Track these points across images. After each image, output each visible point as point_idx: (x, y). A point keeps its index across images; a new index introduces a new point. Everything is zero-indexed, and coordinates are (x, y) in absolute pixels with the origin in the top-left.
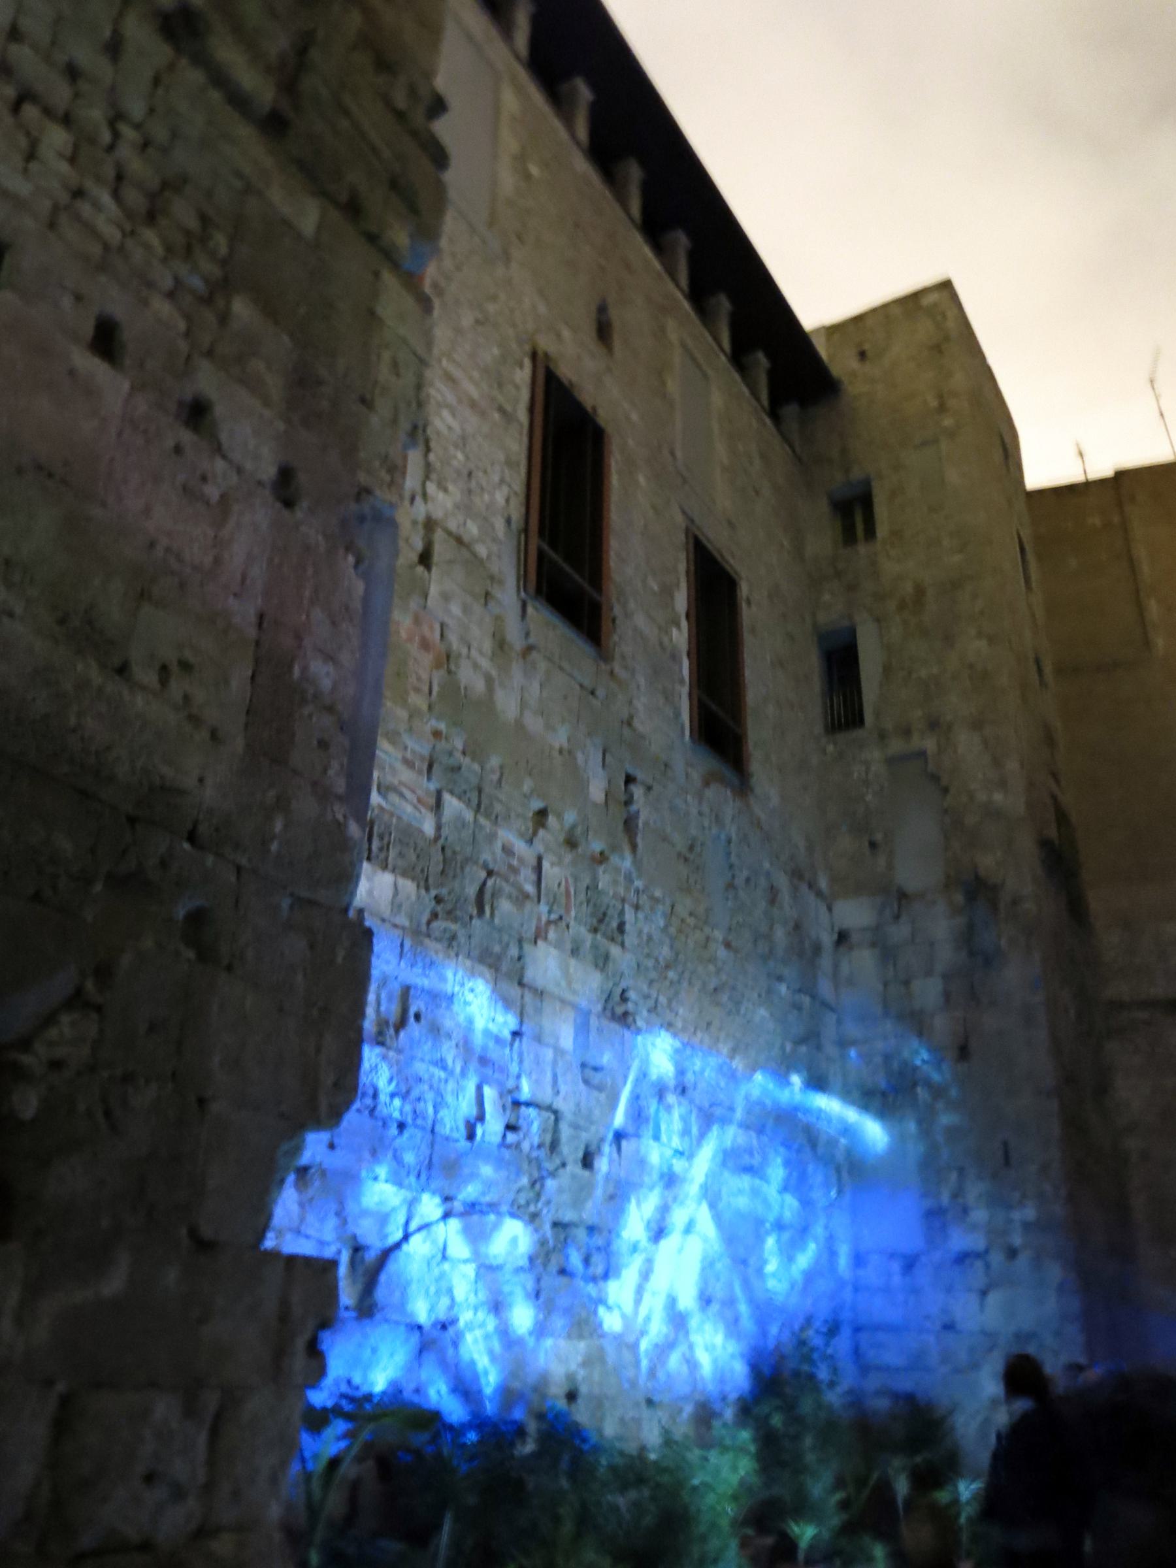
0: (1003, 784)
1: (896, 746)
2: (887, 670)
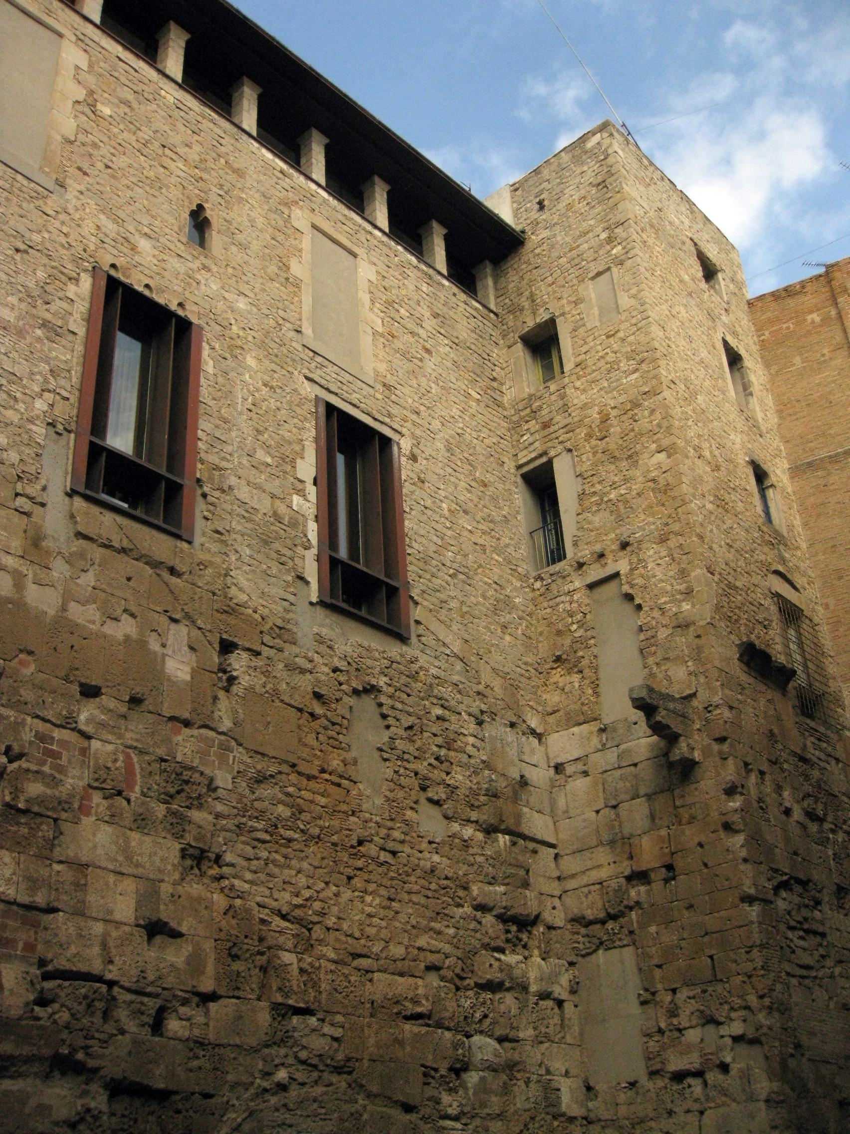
0: (688, 593)
1: (595, 573)
2: (582, 496)
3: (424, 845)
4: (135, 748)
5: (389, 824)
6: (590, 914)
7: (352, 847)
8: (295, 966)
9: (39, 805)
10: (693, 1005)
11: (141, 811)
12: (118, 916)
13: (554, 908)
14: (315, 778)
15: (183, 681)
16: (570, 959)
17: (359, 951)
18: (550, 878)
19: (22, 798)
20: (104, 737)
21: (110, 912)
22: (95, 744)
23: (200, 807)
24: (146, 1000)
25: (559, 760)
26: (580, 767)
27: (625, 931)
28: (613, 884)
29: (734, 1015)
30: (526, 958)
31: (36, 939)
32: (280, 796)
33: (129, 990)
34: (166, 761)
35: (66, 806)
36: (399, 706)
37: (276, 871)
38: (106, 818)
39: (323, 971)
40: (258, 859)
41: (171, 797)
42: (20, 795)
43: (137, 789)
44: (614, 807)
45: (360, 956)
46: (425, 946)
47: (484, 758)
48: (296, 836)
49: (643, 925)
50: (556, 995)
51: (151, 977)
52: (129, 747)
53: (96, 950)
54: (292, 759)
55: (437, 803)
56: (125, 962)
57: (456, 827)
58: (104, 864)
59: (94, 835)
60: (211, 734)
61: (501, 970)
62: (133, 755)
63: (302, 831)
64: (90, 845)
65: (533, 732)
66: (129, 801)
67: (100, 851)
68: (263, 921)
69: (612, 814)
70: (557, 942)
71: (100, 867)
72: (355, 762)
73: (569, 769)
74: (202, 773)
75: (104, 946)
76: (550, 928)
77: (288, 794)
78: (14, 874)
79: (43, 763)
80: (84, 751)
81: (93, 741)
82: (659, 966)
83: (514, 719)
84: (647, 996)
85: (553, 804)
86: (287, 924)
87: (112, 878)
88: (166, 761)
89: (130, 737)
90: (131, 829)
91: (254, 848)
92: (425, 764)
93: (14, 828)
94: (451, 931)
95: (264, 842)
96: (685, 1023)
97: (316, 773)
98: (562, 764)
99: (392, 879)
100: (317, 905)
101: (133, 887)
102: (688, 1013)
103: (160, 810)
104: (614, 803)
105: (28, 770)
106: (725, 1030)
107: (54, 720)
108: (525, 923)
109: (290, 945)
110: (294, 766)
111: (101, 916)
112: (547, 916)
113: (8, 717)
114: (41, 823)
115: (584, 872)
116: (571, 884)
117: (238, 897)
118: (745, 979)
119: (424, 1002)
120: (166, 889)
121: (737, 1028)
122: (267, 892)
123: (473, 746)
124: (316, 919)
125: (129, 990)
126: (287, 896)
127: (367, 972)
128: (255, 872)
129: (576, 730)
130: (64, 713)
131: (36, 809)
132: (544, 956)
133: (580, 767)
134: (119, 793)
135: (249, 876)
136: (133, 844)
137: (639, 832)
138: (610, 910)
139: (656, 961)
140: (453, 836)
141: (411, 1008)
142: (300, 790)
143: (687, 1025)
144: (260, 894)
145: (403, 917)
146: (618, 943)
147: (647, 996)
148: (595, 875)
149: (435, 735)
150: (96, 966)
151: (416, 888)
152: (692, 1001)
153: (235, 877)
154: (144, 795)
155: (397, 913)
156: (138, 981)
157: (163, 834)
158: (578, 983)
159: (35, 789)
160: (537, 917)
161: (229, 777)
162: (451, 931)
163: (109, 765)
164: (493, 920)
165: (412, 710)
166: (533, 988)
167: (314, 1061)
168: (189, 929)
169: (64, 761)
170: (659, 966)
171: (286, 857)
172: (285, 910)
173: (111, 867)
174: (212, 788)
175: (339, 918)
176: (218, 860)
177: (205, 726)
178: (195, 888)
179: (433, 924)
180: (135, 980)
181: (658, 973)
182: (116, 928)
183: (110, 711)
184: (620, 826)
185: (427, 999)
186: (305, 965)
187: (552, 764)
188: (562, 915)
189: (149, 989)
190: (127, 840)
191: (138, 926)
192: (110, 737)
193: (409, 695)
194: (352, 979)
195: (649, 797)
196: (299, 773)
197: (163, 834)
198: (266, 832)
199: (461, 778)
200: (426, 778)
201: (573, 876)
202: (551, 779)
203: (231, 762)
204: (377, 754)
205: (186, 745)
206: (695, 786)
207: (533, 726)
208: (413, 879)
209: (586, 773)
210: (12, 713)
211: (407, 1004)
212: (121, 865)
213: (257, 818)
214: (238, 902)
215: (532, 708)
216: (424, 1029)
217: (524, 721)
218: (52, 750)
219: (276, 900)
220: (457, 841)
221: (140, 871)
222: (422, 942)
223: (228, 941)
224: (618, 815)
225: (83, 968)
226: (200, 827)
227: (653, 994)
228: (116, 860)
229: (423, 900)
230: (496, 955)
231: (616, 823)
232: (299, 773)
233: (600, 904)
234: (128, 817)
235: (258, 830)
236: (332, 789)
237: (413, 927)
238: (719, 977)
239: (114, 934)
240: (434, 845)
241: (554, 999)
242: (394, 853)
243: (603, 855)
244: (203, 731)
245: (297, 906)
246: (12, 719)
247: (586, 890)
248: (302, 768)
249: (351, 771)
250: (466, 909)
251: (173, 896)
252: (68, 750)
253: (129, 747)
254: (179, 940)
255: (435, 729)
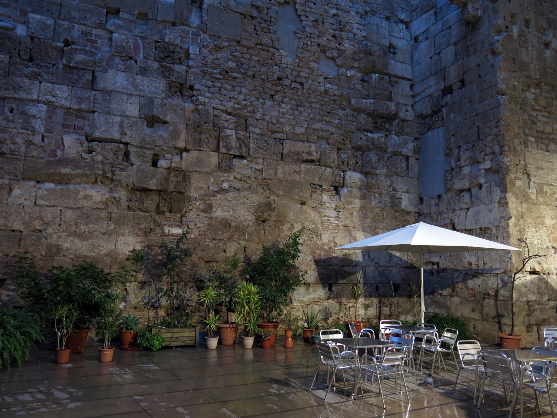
3: (321, 79)
4: (140, 36)
5: (298, 69)
6: (425, 112)
7: (274, 80)
8: (234, 136)
9: (83, 64)
10: (467, 154)
11: (143, 65)
12: (128, 114)
13: (407, 111)
14: (252, 48)
15: (170, 3)
16: (415, 136)
17: (275, 129)
18: (405, 96)
19: (72, 62)
20: (121, 32)
21: (124, 112)
22: (115, 35)
23: (181, 63)
24: (145, 151)
25: (416, 34)
26: (425, 35)
27: (440, 119)
28: (436, 95)
29: (486, 158)
30: (387, 136)
31: (84, 125)
32: (230, 57)
33: (136, 147)
34: (159, 42)
35: (99, 65)
36: (308, 10)
37: (225, 92)
38: (122, 70)
39: (251, 138)
40: (215, 87)
41: (163, 59)
42: (71, 60)
43: (141, 56)
44: (439, 53)
45: (275, 132)
46: (318, 128)
47: (364, 35)
48: (239, 76)
49: (448, 115)
50: (404, 153)
51: (147, 140)
52: (135, 36)
53: (117, 128)
54: (238, 38)
55: (333, 59)
56: (133, 134)
57: (343, 70)
58: (120, 90)
59: (115, 77)
60: (189, 28)
61: (367, 141)
62: (139, 40)
63: (243, 73)
64: (113, 82)
65: (402, 22)
66: (136, 62)
67: (118, 84)
68: (214, 116)
69: (436, 57)
70: (407, 128)
71: (119, 92)
72: (278, 40)
73: (420, 38)
74: (181, 48)
75: (121, 126)
76: (403, 121)
77: (234, 56)
78: (69, 96)
79: (86, 46)
80: (111, 39)
81: (114, 34)
82: (454, 135)
83: (389, 14)
84: (448, 151)
85: (412, 57)
86: (231, 117)
87: (125, 97)
88: (159, 42)
89: (136, 32)
90: (137, 74)
91: (212, 82)
92: (325, 39)
93: (71, 76)
94: (337, 121)
95: (218, 79)
96: (463, 164)
97: (253, 46)
98: (417, 36)
99: (299, 96)
100: (250, 109)
101: (137, 100)
102: (465, 158)
103: (156, 65)
104: (438, 51)
105: (76, 49)
106: (482, 166)
107: (91, 25)
108: (390, 118)
109: (231, 126)
110: (238, 42)
111: (119, 113)
112: (402, 115)
113: (64, 25)
114: (85, 73)
115: (423, 91)
116: (418, 98)
117: (201, 104)
118: (495, 138)
119: (314, 154)
120: (157, 102)
121: (488, 165)
122: (220, 102)
123: (357, 28)
124: (249, 114)
125: (136, 147)
126: (231, 104)
127: (280, 139)
128: (213, 93)
129: (424, 16)
130: (97, 21)
131: (81, 66)
132: (398, 134)
133: (425, 35)
134: (131, 58)
135: (208, 95)
136: (138, 81)
137: (449, 65)
138: (434, 109)
139: (452, 133)
140: (342, 75)
141: (305, 157)
142: (242, 54)
143: (464, 165)
144: (216, 103)
145: (305, 114)
146: (437, 126)
147: (448, 151)
148: (428, 92)
149: (332, 24)
150: (116, 135)
151: (314, 100)
152: (467, 152)
153: (200, 95)
154: (144, 58)
155: (301, 112)
156: (141, 142)
157: (156, 76)
158: (419, 148)
159: (80, 57)
160: (396, 114)
161: (198, 49)
162: (337, 121)
163: (124, 44)
164: (365, 116)
165: (316, 11)
166: (390, 149)
167: (244, 179)
168: (171, 119)
169: (99, 44)
170: (454, 135)
171: (232, 86)
172: (230, 110)
173: (124, 91)
174: (188, 54)
175: (264, 114)
176: (191, 88)
177: (184, 25)
178: (176, 101)
179: (324, 118)
180: (138, 142)
181: (453, 139)
182: (128, 119)
183: (125, 19)
184: (441, 63)
185: (317, 153)
186: (240, 136)
187: (413, 38)
188: (413, 114)
189: (147, 146)
190: (134, 80)
191: (140, 118)
192: (124, 32)
193: (315, 4)
194: (270, 143)
195: (455, 44)
196: (242, 46)
197: (156, 76)
198: (221, 74)
199: (348, 45)
200: (324, 46)
201: (419, 94)
202: (412, 46)
203: (199, 41)
204: (293, 35)
205: (171, 36)
206: (477, 32)
207: (402, 18)
208: (313, 96)
209: (427, 38)
210: (66, 23)
211: (304, 155)
212: (131, 91)
213: (216, 68)
214: (201, 107)
215: (403, 8)
216: (313, 167)
217: (396, 16)
218: (92, 39)
219: (225, 106)
220: (343, 77)
221: (142, 93)
222: (317, 126)
223: (195, 125)
224: (440, 57)
225: (109, 137)
226: (179, 72)
227: (451, 150)
228: (128, 89)
229: (318, 106)
230: (365, 133)
231: (439, 62)
232: (242, 46)
233: (429, 107)
234: (135, 68)
235: (215, 74)
236: (261, 53)
237: (312, 119)
238: (481, 138)
239: (126, 121)
240: (328, 80)
241: (403, 156)
242: (302, 84)
243: (432, 81)
244: (182, 27)
245: (237, 109)
246: (66, 26)
247: (423, 100)
248: (244, 43)
249: (276, 44)
250: (347, 111)
251: (161, 105)
252: (101, 39)
253: (135, 36)
254: (166, 125)
255: (331, 21)
